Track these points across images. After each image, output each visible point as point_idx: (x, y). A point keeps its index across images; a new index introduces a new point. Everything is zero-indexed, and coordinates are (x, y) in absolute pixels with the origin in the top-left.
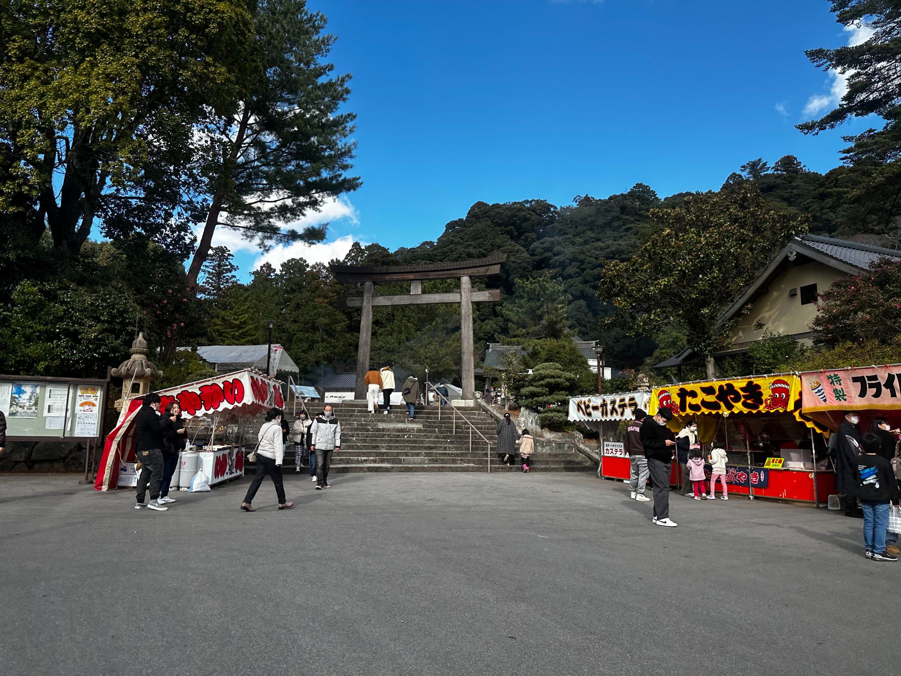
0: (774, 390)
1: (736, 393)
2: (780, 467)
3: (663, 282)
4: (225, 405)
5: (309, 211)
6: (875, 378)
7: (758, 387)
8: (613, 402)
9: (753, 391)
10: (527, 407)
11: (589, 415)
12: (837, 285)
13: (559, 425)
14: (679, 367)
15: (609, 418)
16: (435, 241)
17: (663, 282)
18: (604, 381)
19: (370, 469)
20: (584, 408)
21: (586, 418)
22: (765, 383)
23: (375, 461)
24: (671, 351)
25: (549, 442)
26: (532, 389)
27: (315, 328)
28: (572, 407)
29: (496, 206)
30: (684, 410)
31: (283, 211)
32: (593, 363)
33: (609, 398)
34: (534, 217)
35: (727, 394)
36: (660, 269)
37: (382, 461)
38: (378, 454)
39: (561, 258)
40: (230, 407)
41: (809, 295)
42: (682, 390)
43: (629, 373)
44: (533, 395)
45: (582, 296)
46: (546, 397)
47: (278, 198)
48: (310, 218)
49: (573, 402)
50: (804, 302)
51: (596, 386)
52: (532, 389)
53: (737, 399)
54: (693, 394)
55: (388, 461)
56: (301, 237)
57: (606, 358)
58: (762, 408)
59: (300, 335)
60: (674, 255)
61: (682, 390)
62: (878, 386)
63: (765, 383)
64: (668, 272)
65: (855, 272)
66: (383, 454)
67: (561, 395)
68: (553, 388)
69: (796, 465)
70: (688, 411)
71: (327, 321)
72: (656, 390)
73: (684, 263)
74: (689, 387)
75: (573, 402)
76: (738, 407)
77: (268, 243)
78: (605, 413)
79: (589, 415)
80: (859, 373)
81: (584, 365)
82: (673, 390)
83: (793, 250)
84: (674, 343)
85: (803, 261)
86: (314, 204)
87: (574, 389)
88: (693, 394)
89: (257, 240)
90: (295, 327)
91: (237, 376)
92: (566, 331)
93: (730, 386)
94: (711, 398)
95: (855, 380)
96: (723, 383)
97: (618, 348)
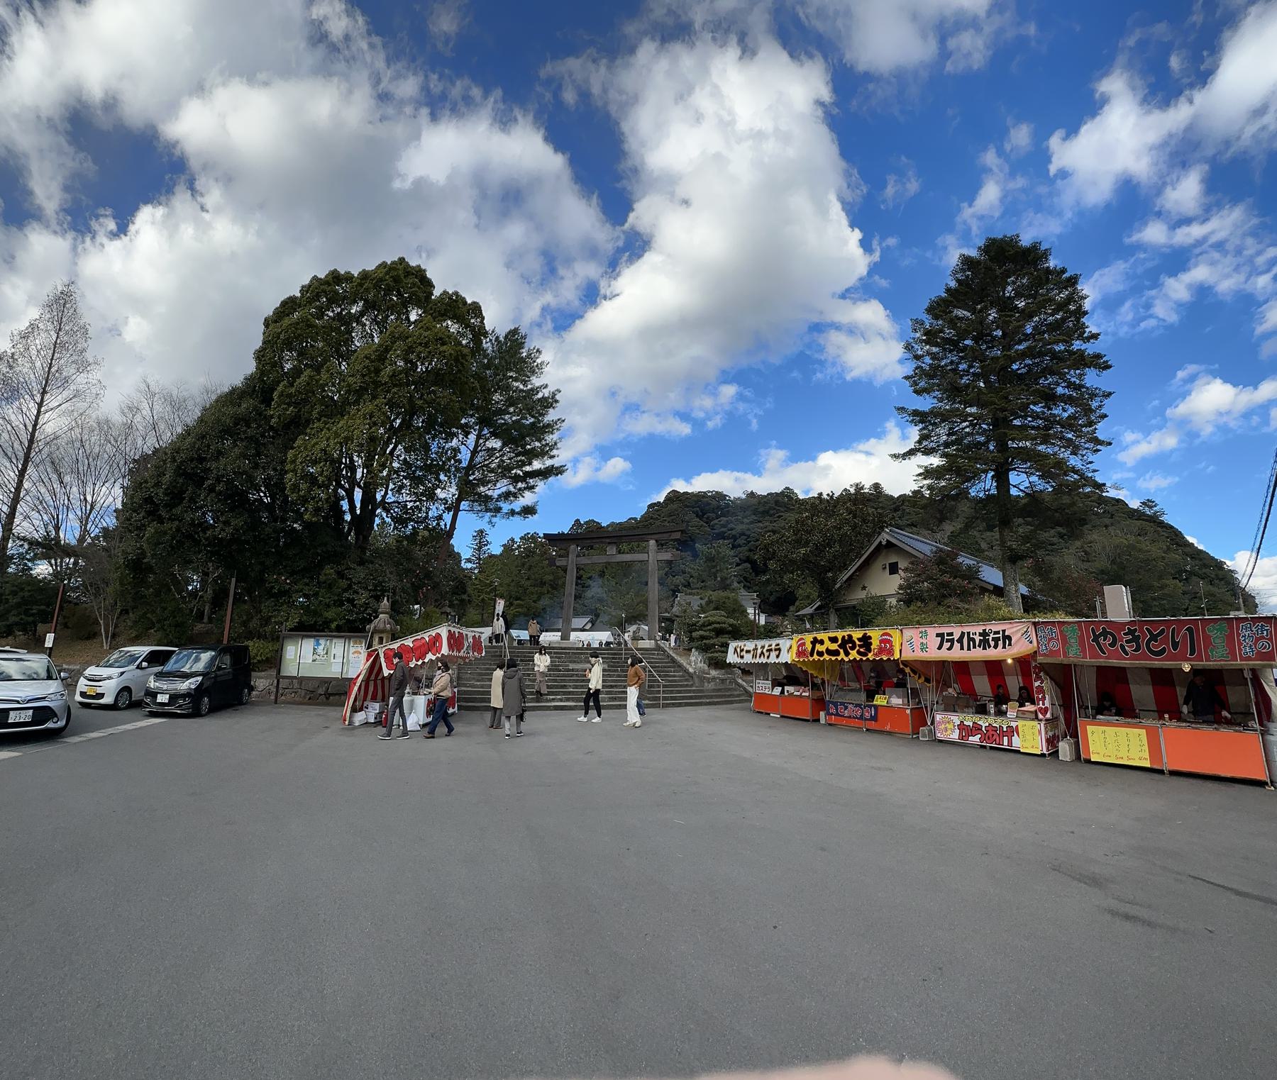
0: (881, 641)
1: (854, 643)
2: (885, 703)
3: (803, 551)
4: (430, 656)
5: (527, 494)
6: (951, 634)
7: (870, 638)
8: (763, 647)
9: (866, 640)
10: (697, 648)
11: (742, 657)
12: (912, 563)
13: (720, 664)
14: (812, 615)
15: (758, 660)
16: (639, 517)
17: (803, 551)
18: (758, 626)
19: (556, 708)
20: (739, 653)
21: (739, 660)
22: (875, 635)
23: (561, 700)
24: (806, 602)
25: (714, 678)
26: (701, 633)
27: (543, 584)
28: (731, 649)
29: (686, 493)
30: (812, 655)
31: (507, 496)
32: (750, 611)
33: (760, 643)
34: (714, 503)
35: (847, 643)
36: (799, 543)
37: (568, 700)
38: (565, 693)
39: (734, 532)
40: (434, 658)
41: (894, 569)
42: (815, 639)
43: (776, 619)
44: (702, 638)
45: (748, 560)
46: (710, 639)
47: (503, 486)
48: (528, 499)
49: (733, 645)
50: (891, 573)
51: (752, 632)
52: (701, 633)
53: (853, 648)
54: (822, 642)
55: (573, 700)
56: (519, 513)
57: (763, 607)
58: (870, 656)
59: (531, 589)
60: (808, 532)
61: (815, 639)
62: (952, 641)
63: (875, 635)
64: (806, 544)
65: (921, 556)
66: (570, 693)
67: (721, 640)
68: (719, 632)
69: (897, 701)
70: (816, 657)
71: (551, 577)
72: (796, 637)
73: (817, 538)
74: (819, 637)
75: (733, 645)
76: (854, 654)
77: (494, 520)
78: (754, 656)
79: (742, 657)
80: (940, 631)
81: (744, 613)
82: (808, 638)
83: (885, 537)
84: (808, 597)
85: (890, 545)
86: (531, 488)
87: (737, 634)
88: (822, 642)
89: (487, 518)
90: (528, 583)
91: (438, 631)
92: (736, 584)
93: (850, 636)
94: (834, 647)
95: (938, 635)
96: (845, 634)
97: (772, 599)
